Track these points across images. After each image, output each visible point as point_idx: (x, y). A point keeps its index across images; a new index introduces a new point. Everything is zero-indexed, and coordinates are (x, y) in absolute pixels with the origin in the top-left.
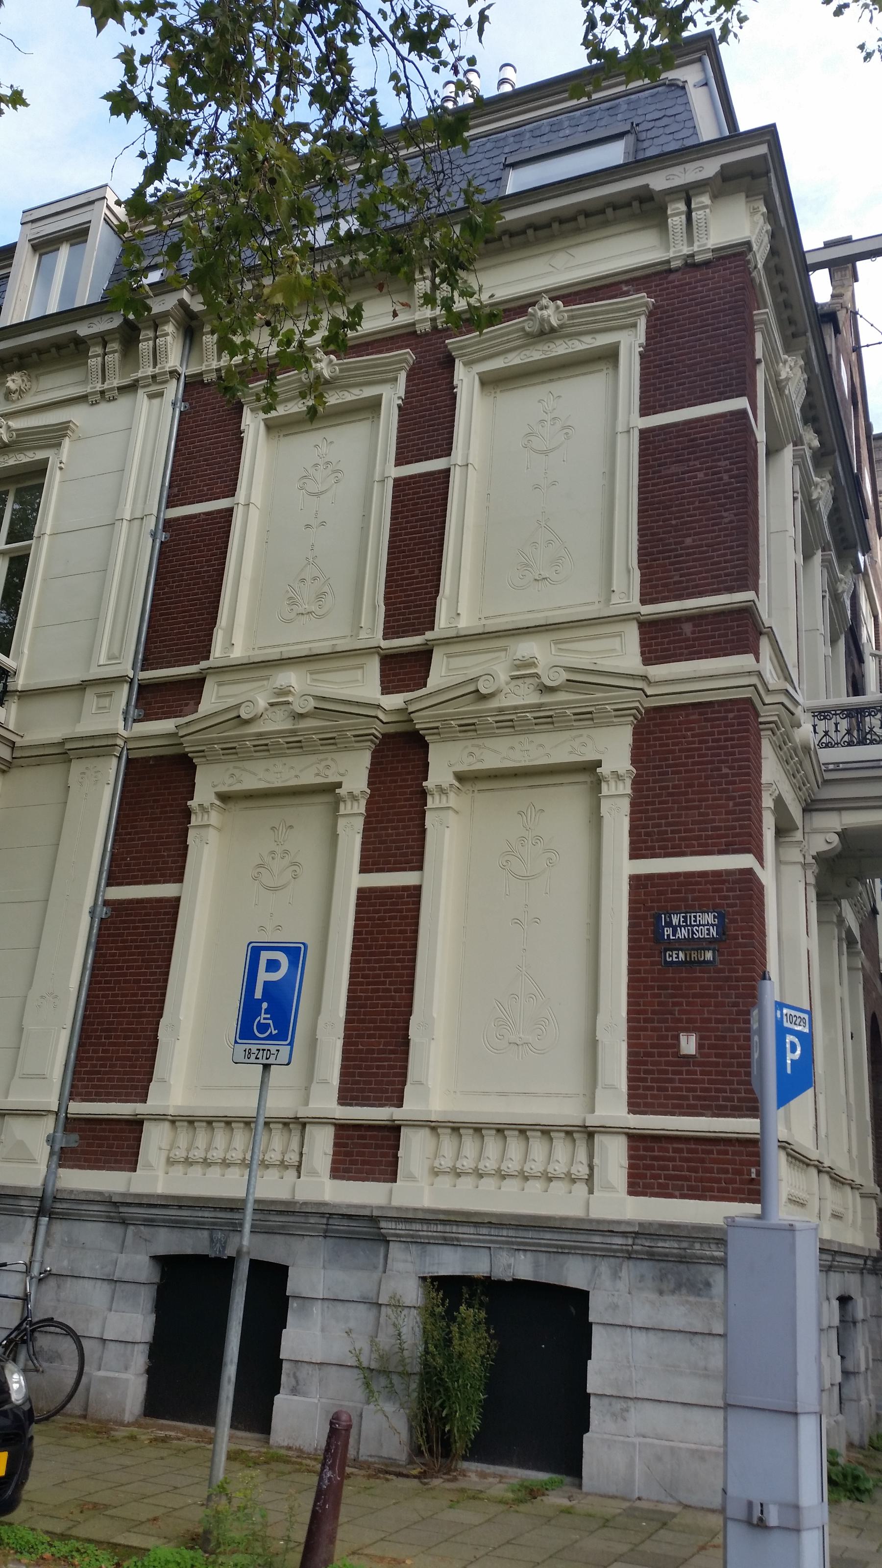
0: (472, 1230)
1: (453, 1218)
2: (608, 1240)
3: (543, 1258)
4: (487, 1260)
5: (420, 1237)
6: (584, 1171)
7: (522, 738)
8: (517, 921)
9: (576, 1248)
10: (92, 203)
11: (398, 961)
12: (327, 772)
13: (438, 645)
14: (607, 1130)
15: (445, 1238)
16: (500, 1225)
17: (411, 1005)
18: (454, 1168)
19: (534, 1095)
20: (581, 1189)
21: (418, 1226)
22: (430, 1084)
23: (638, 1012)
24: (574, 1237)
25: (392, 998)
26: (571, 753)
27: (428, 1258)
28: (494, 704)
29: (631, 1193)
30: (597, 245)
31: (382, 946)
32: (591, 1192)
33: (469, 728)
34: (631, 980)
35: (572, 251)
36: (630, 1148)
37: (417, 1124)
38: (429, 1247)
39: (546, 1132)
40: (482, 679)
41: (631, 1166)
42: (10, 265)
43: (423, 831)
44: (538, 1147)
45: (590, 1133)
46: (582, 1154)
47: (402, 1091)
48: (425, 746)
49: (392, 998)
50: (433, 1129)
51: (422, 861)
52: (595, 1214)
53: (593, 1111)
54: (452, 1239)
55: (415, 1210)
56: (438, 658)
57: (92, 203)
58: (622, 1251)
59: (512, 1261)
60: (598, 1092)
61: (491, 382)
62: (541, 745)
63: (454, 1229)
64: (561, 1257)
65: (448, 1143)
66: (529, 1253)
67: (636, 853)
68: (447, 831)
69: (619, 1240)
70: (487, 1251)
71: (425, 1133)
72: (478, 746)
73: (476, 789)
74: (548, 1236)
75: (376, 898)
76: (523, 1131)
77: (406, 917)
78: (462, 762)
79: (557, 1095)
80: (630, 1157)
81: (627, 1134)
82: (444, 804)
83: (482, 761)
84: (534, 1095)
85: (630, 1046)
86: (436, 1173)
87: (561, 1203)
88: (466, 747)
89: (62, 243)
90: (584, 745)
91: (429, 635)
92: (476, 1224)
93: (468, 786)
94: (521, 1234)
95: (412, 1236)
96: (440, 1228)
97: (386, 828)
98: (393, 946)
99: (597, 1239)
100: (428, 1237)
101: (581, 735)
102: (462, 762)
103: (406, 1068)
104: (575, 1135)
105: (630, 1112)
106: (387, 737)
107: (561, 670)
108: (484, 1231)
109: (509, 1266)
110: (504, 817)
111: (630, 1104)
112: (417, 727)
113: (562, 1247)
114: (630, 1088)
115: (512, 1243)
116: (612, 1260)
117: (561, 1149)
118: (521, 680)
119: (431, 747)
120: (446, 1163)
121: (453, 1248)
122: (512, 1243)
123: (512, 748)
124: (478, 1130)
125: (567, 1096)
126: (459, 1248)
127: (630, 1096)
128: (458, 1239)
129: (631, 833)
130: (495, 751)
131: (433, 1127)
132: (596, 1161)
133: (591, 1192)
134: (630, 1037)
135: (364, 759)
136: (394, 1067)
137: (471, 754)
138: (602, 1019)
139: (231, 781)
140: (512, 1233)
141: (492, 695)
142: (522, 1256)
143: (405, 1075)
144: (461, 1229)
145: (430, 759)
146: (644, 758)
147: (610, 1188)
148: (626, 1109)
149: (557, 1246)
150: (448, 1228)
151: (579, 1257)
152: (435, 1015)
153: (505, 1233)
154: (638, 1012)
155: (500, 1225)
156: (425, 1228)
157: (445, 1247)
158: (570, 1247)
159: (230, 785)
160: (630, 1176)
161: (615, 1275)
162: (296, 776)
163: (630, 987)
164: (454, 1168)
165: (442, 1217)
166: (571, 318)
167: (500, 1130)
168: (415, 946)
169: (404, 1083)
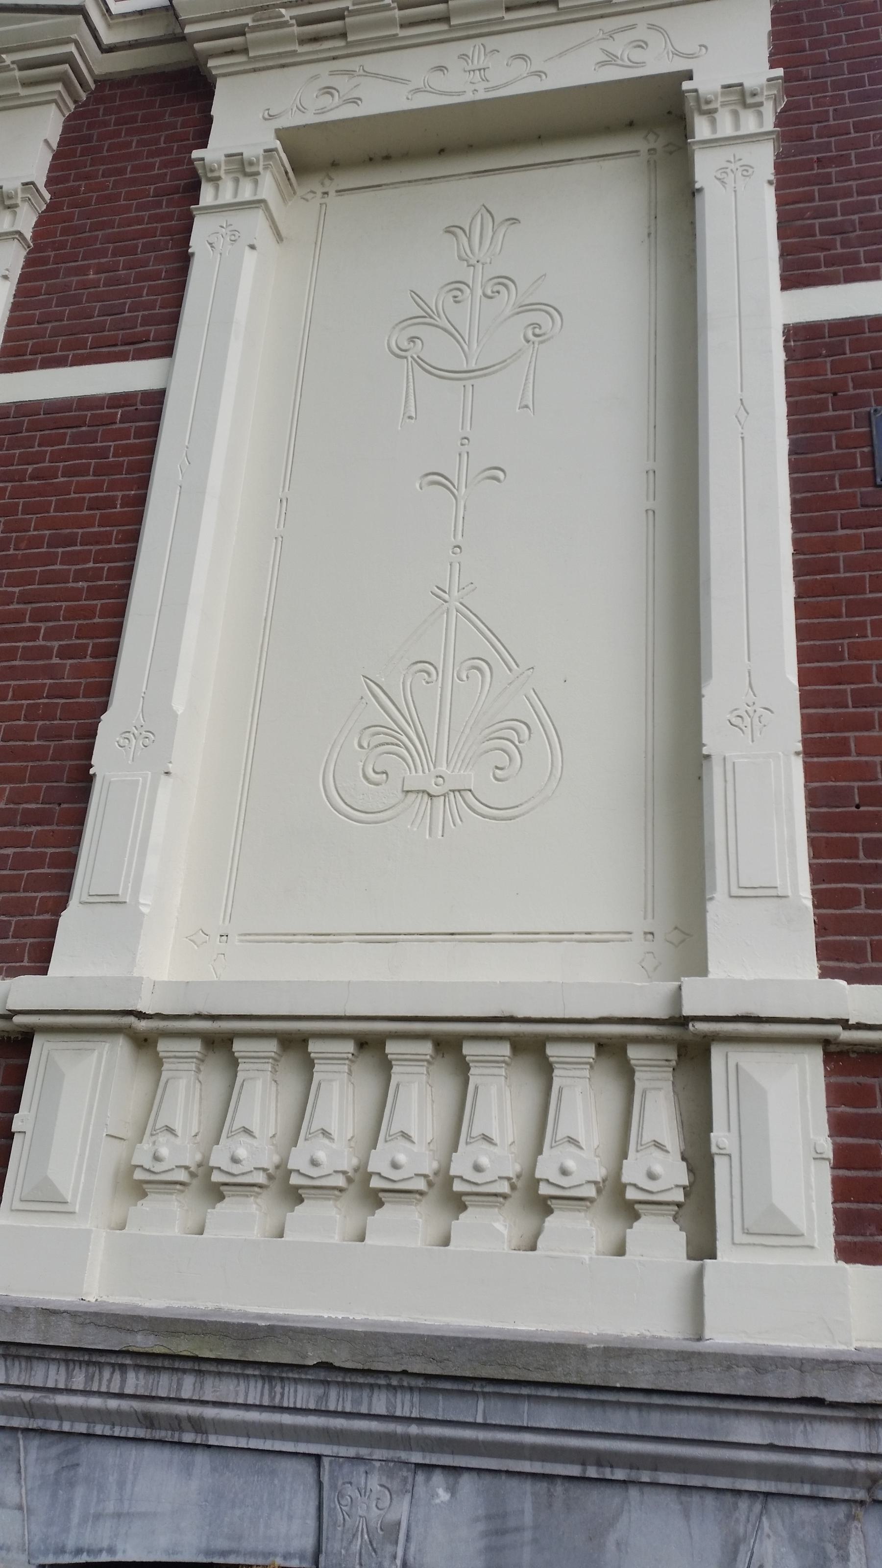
0: (255, 1392)
1: (183, 1347)
2: (797, 1435)
3: (523, 1500)
4: (302, 1504)
5: (59, 1412)
6: (671, 1175)
7: (466, 46)
8: (438, 479)
9: (656, 1463)
11: (80, 576)
14: (758, 1030)
15: (149, 1420)
16: (366, 1377)
17: (105, 690)
18: (204, 1170)
19: (483, 936)
20: (660, 1242)
21: (55, 1376)
22: (146, 901)
23: (834, 677)
24: (655, 1423)
25: (51, 672)
26: (603, 64)
27: (80, 1492)
29: (850, 1251)
31: (36, 542)
32: (703, 1248)
34: (803, 592)
36: (836, 1095)
37: (83, 1026)
38: (91, 1452)
39: (531, 1045)
41: (843, 1159)
43: (185, 260)
44: (500, 1097)
45: (690, 1045)
46: (659, 1113)
47: (51, 930)
49: (51, 672)
50: (144, 1043)
51: (172, 336)
52: (725, 1332)
53: (702, 970)
54: (177, 1423)
55: (49, 1313)
58: (849, 1478)
59: (401, 1510)
60: (719, 911)
61: (314, 158)
62: (522, 57)
63: (188, 1386)
64: (595, 1497)
65: (188, 1089)
66: (466, 1482)
67: (797, 274)
68: (250, 259)
69: (842, 1437)
70: (306, 1469)
71: (115, 1052)
72: (349, 73)
73: (331, 187)
74: (551, 1416)
75: (35, 426)
76: (450, 1043)
77: (116, 468)
78: (302, 109)
79: (557, 936)
80: (839, 1126)
81: (826, 1042)
82: (247, 192)
83: (356, 101)
84: (483, 936)
85: (810, 773)
86: (137, 1186)
87: (599, 1292)
88: (316, 77)
90: (642, 45)
92: (272, 1372)
93: (315, 184)
94: (441, 1408)
95: (29, 1410)
96: (134, 1382)
97: (83, 270)
98: (70, 541)
99: (749, 1430)
100: (87, 1414)
101: (633, 27)
102: (302, 109)
103: (72, 861)
104: (634, 1053)
105: (826, 973)
106: (108, 87)
108: (302, 1395)
109: (391, 1531)
110: (409, 238)
111: (824, 951)
113: (601, 1459)
114: (820, 899)
115: (407, 1442)
116: (804, 1512)
117: (583, 1099)
120: (176, 1153)
121: (178, 1455)
122: (407, 1442)
124: (295, 1042)
125: (588, 937)
126: (201, 1458)
127: (822, 927)
128: (197, 1425)
129: (783, 232)
130: (393, 79)
131: (142, 1034)
132: (721, 1137)
133: (703, 1248)
134: (810, 749)
135: (46, 126)
136: (38, 860)
137: (328, 90)
138: (718, 700)
140: (405, 1405)
142: (439, 1490)
143: (66, 883)
144: (213, 1389)
145: (216, 110)
146: (808, 70)
147: (779, 1233)
148: (811, 967)
149: (582, 1457)
150: (164, 1384)
151: (668, 1499)
152: (179, 706)
153: (380, 1404)
154: (834, 677)
155: (366, 1377)
156: (79, 1380)
157: (149, 1453)
158: (634, 1462)
160: (842, 1190)
161: (428, 1480)
163: (801, 609)
164: (204, 1170)
165: (143, 1342)
167: (371, 1043)
168: (135, 537)
169: (62, 904)
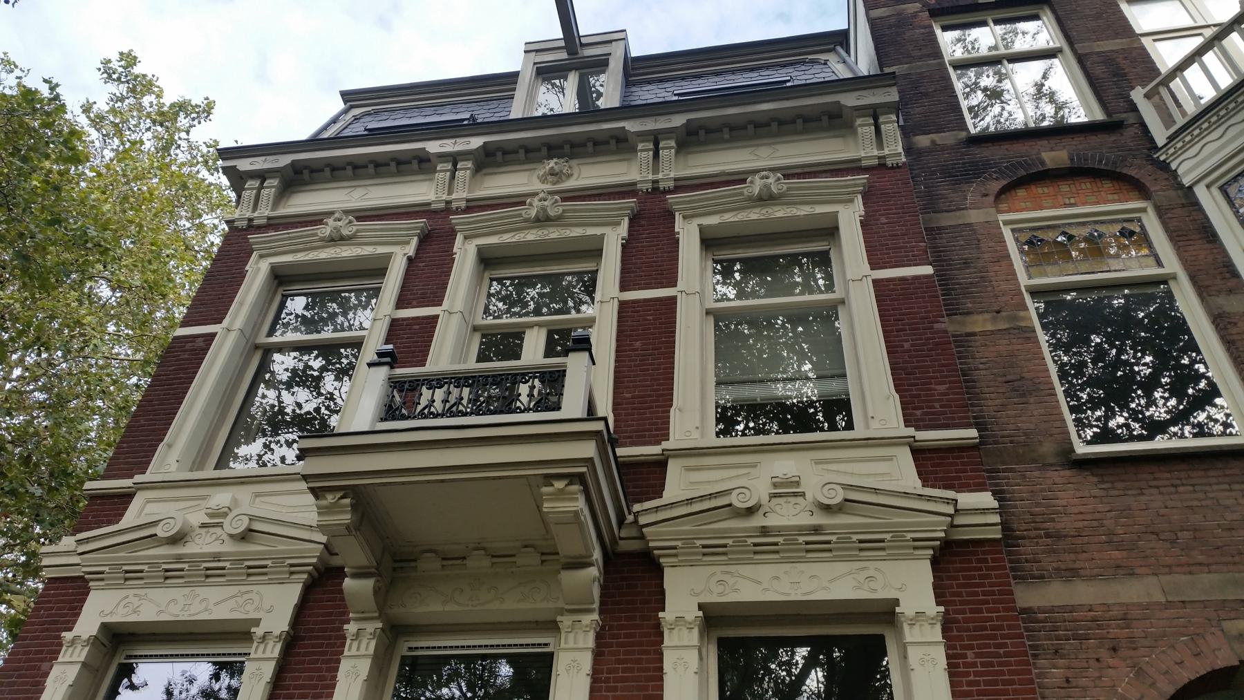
7: (787, 567)
10: (610, 42)
12: (873, 585)
13: (675, 456)
28: (757, 521)
30: (803, 143)
33: (714, 551)
35: (777, 147)
40: (735, 493)
42: (514, 89)
48: (658, 571)
56: (673, 467)
57: (610, 42)
78: (711, 592)
89: (571, 70)
91: (665, 445)
102: (711, 592)
107: (838, 488)
112: (651, 544)
118: (784, 499)
119: (668, 574)
123: (777, 578)
139: (721, 589)
141: (750, 511)
159: (720, 594)
162: (824, 588)
166: (789, 189)
